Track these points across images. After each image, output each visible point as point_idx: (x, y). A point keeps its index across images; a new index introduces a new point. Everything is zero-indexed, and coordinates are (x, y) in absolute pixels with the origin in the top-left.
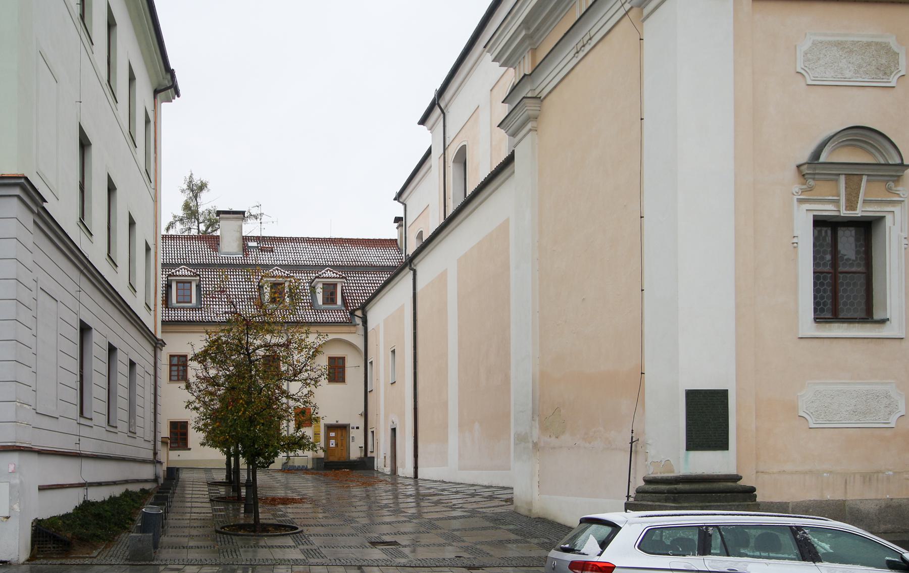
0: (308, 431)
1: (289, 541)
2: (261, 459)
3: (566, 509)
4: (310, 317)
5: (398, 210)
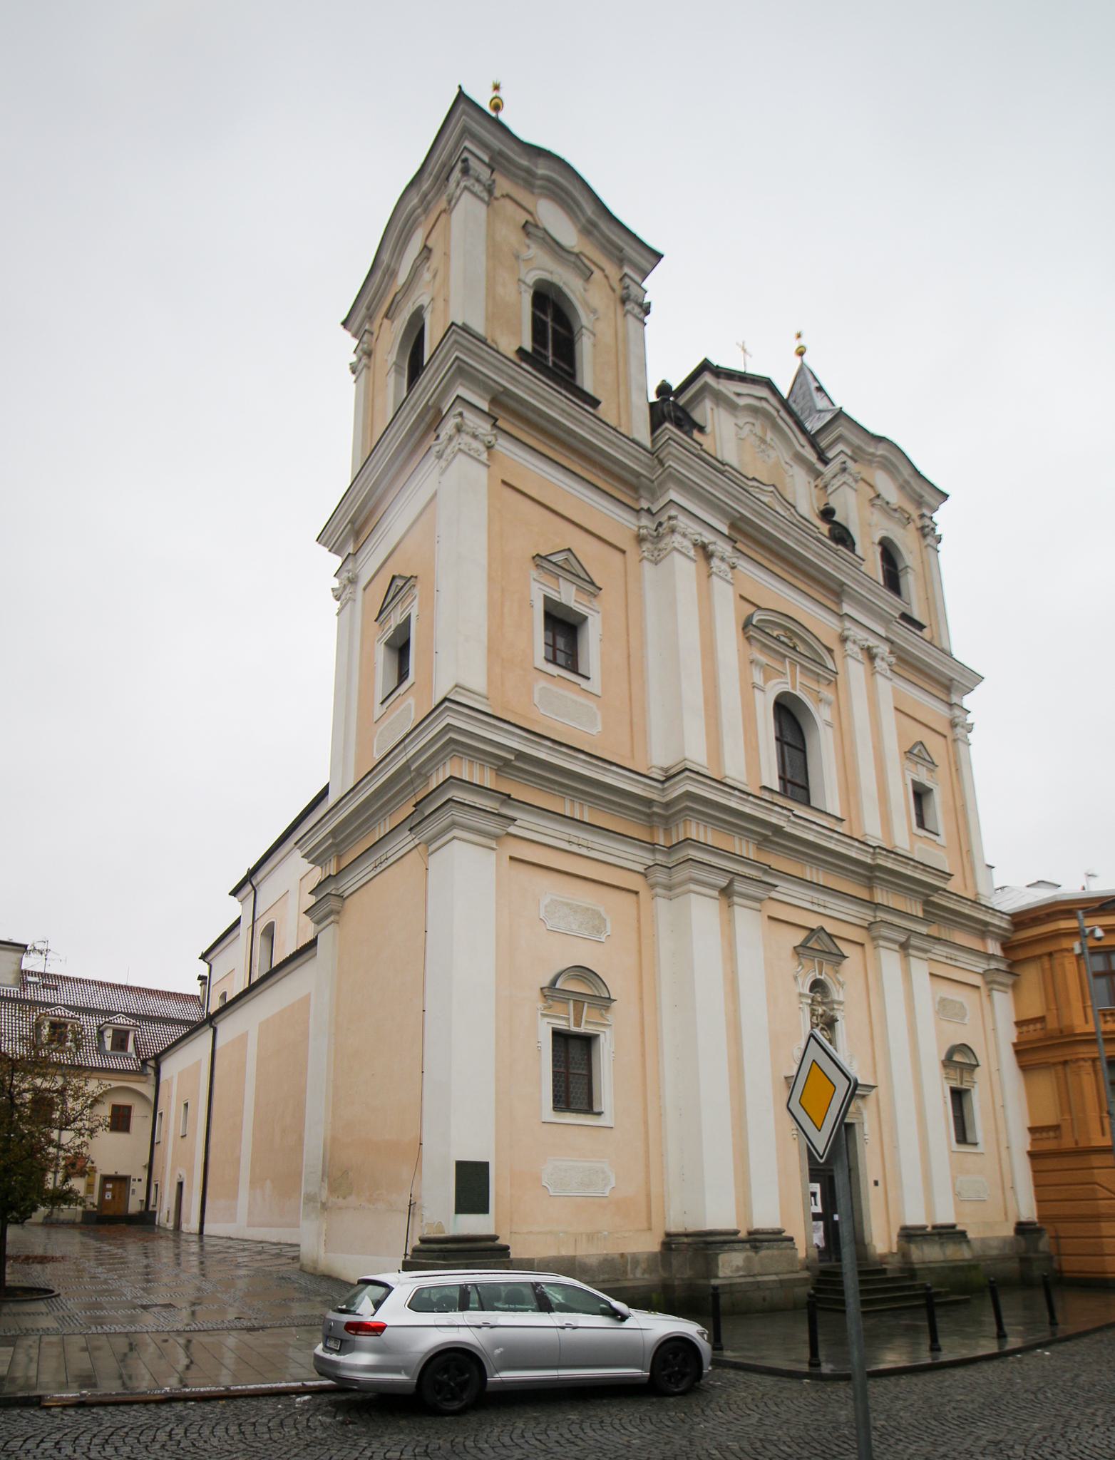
0: (78, 1184)
1: (41, 1306)
2: (15, 1214)
3: (350, 1267)
4: (95, 1061)
5: (203, 969)
